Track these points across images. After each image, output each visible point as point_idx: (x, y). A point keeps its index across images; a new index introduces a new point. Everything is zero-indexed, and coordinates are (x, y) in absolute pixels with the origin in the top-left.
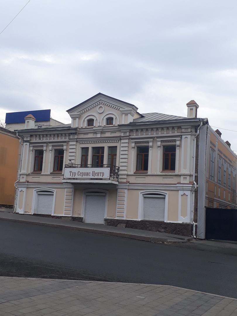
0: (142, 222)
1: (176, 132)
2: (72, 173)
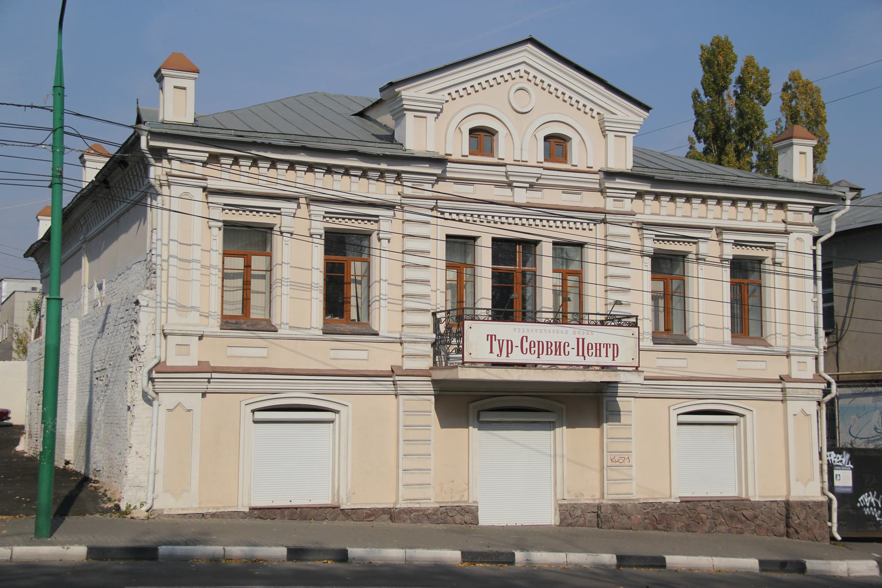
2: (496, 344)
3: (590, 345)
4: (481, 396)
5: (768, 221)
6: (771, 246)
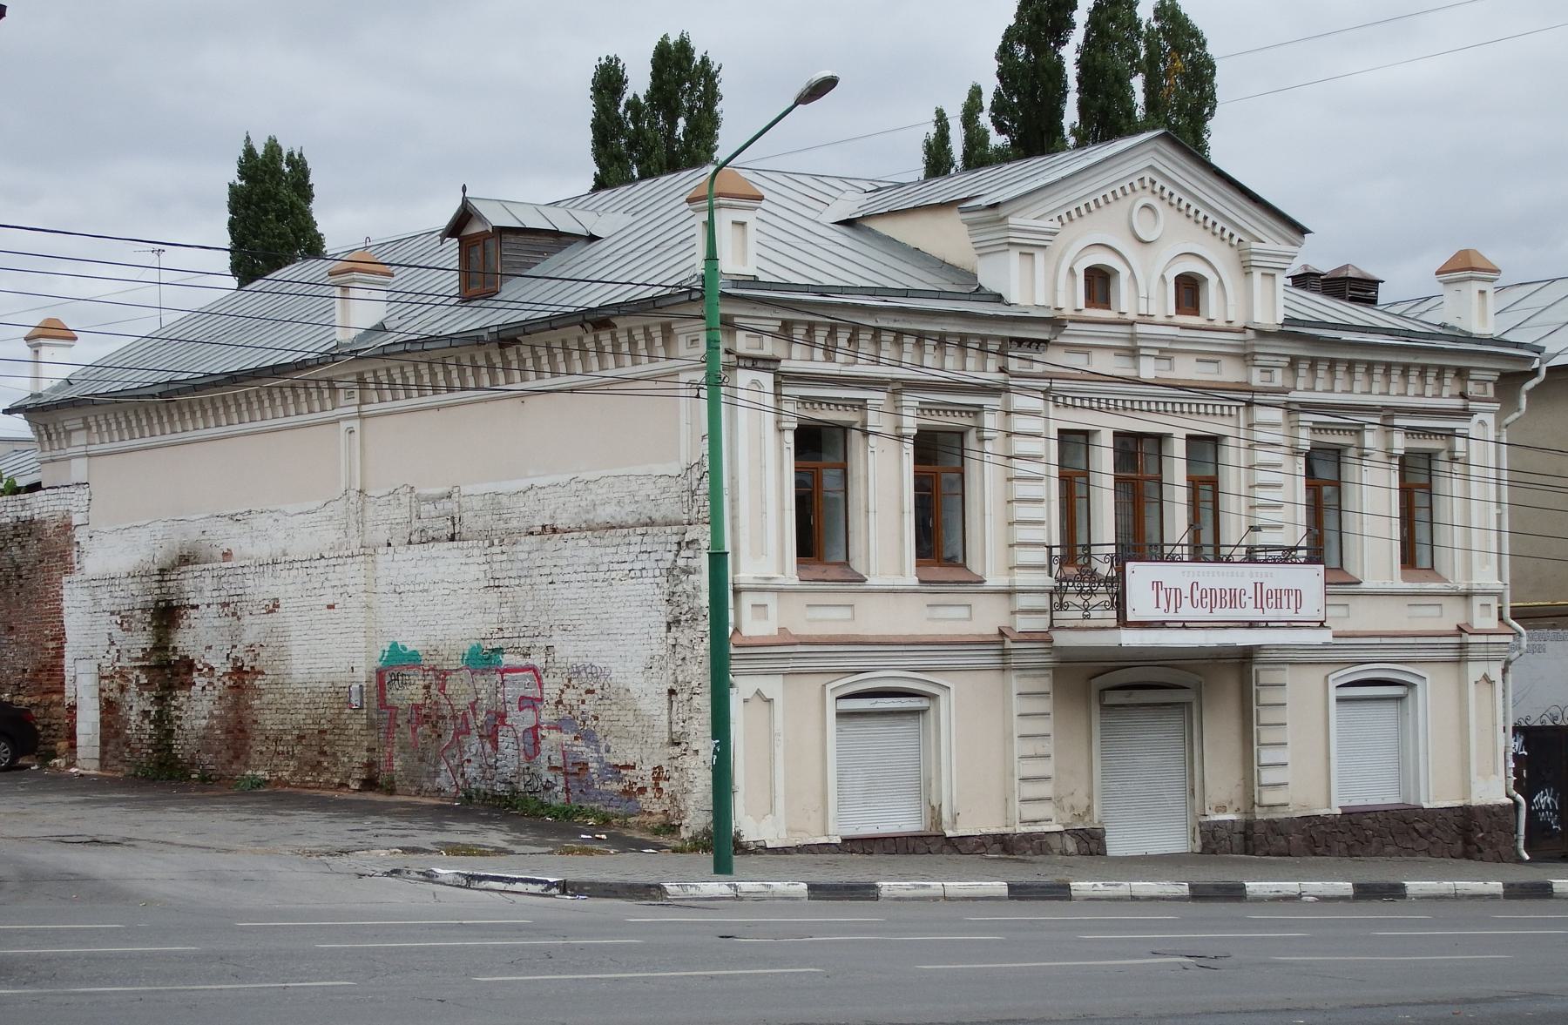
2: (1162, 594)
3: (1270, 592)
6: (1451, 434)
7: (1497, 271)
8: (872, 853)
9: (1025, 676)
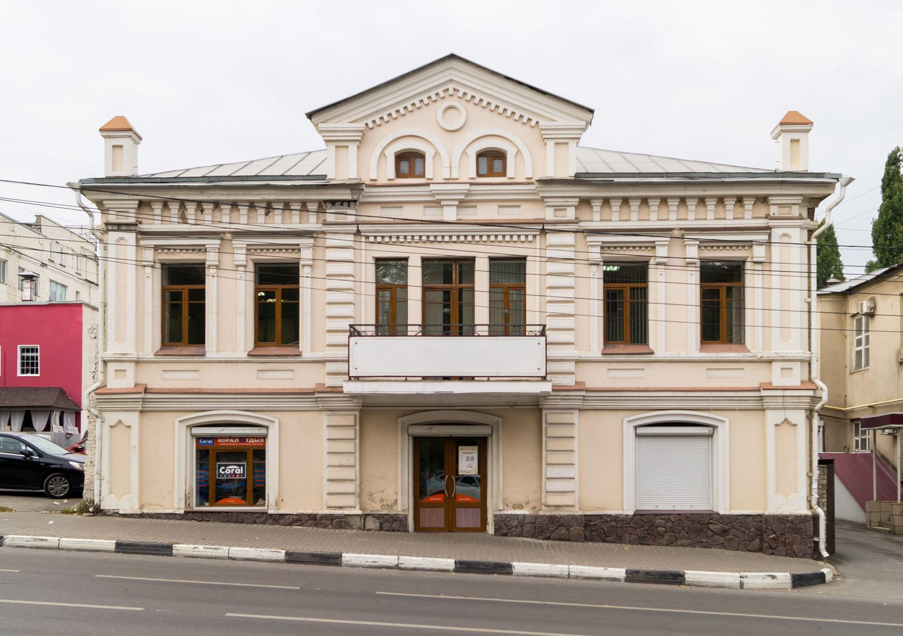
0: (638, 517)
1: (748, 215)
4: (415, 410)
5: (746, 218)
7: (812, 123)
8: (209, 521)
9: (334, 415)
